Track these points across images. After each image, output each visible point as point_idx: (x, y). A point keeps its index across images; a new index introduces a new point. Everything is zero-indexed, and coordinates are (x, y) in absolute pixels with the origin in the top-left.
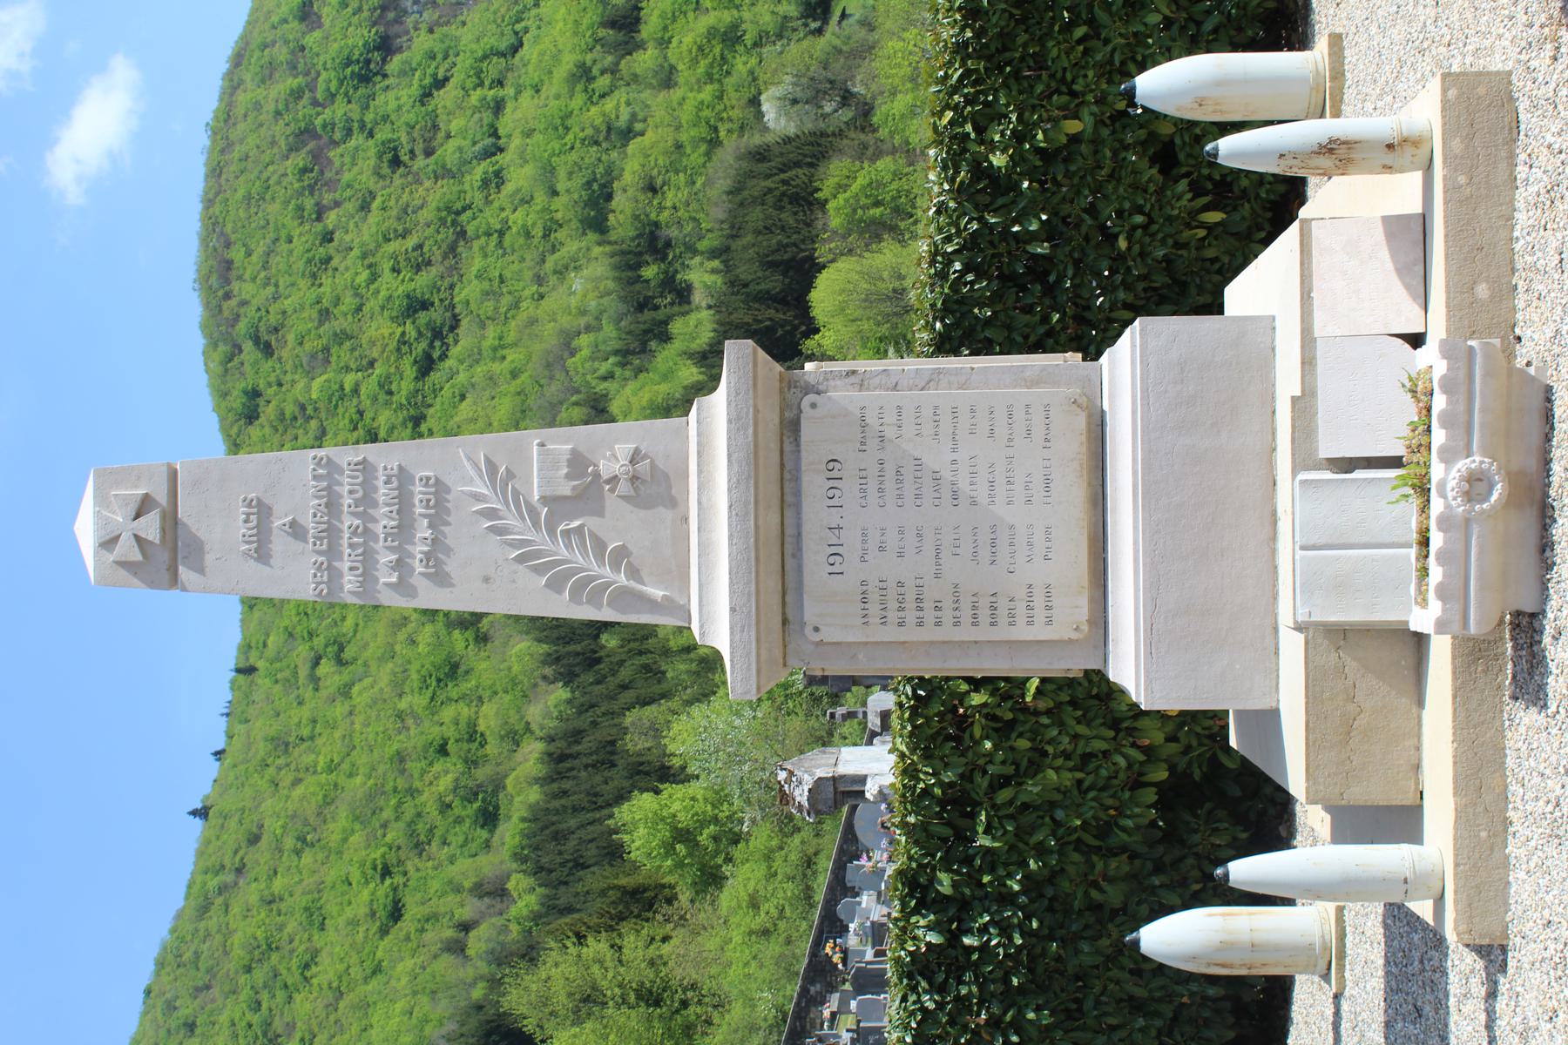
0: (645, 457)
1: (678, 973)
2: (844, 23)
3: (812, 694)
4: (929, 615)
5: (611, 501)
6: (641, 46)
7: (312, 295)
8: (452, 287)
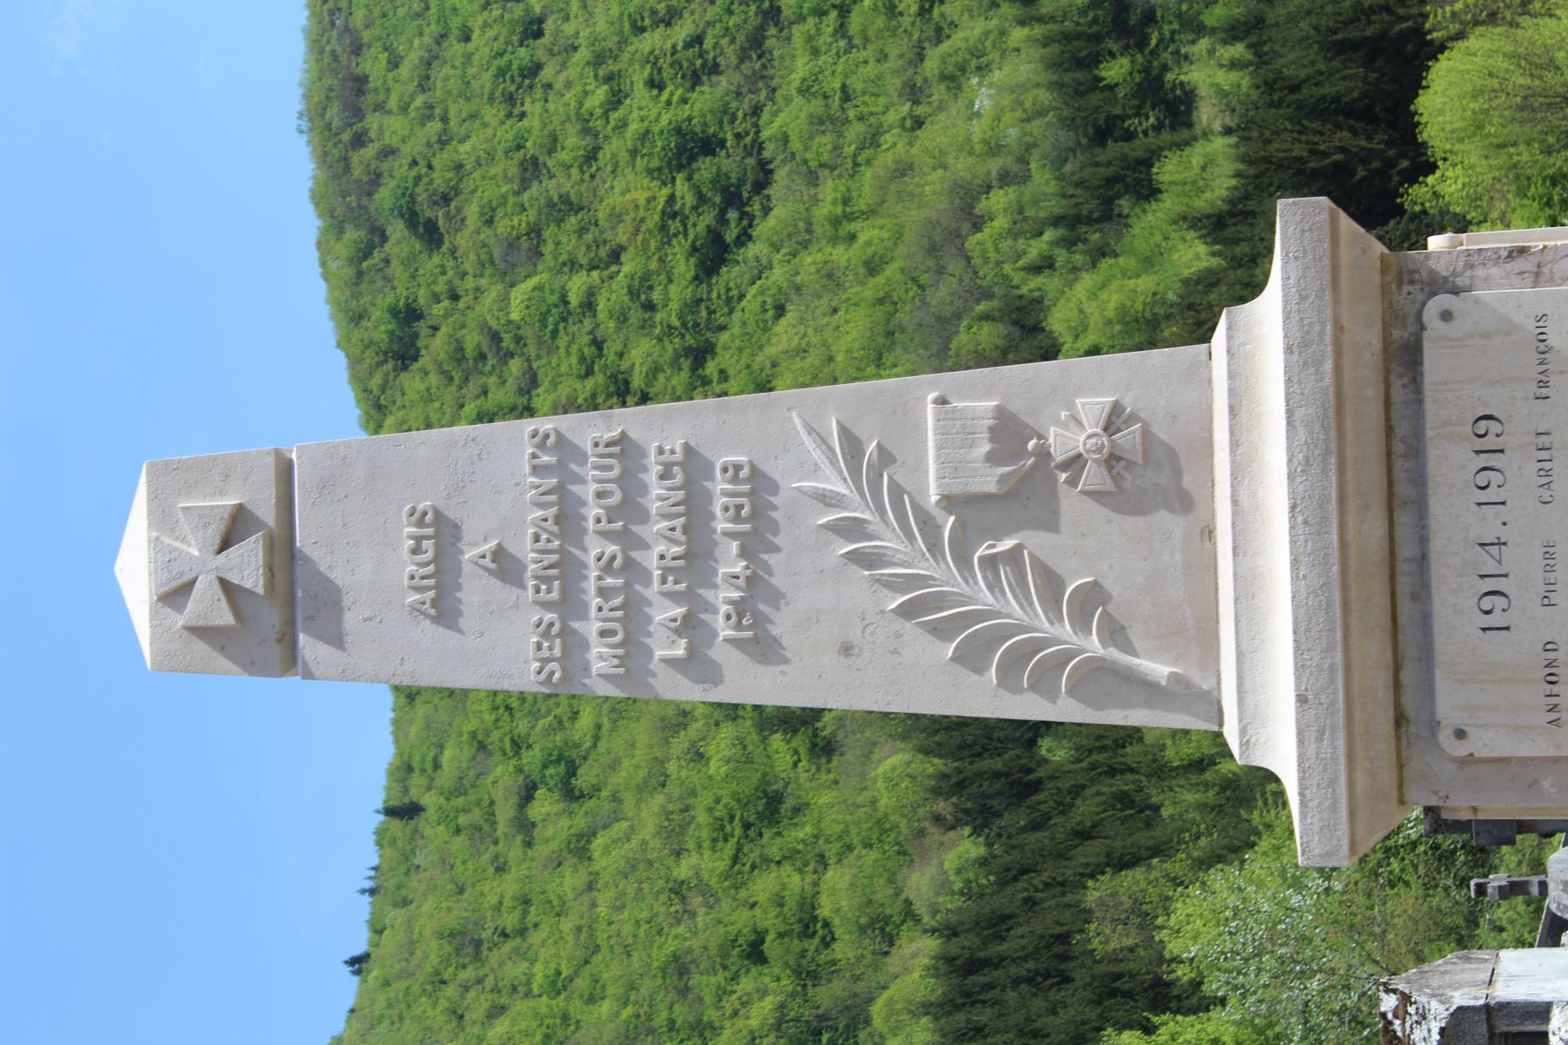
0: (1133, 418)
3: (1435, 847)
5: (1071, 503)
7: (507, 134)
8: (756, 111)
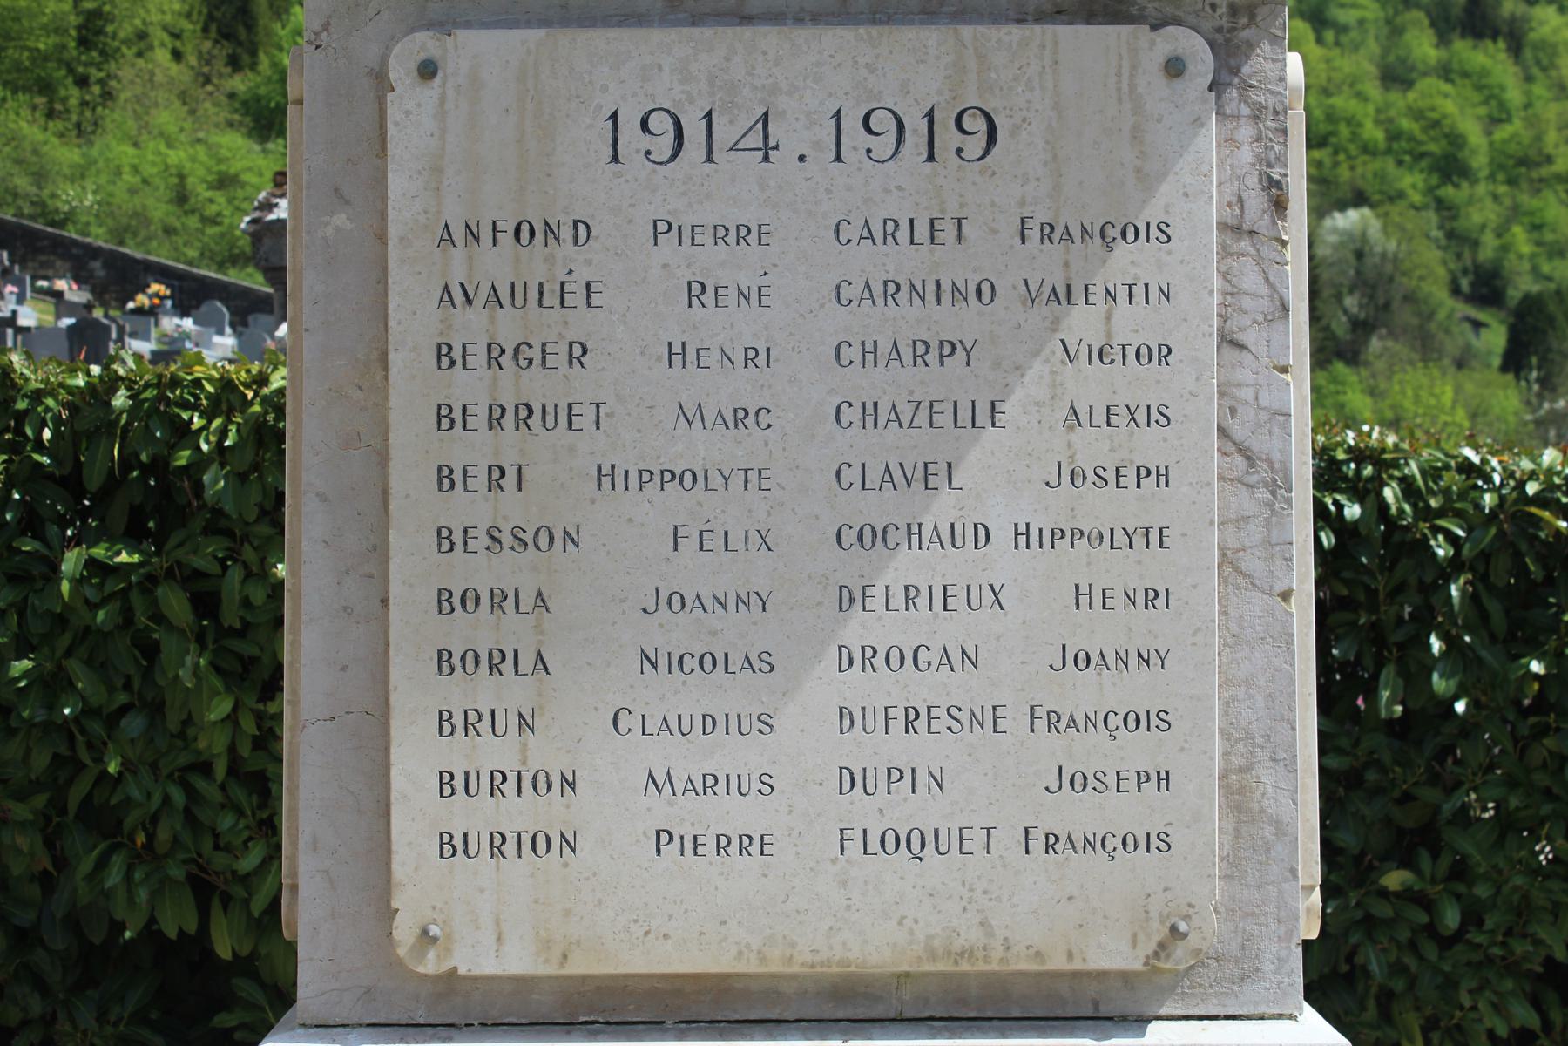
1: (126, 73)
2: (1467, 326)
4: (474, 448)
6: (1443, 40)
